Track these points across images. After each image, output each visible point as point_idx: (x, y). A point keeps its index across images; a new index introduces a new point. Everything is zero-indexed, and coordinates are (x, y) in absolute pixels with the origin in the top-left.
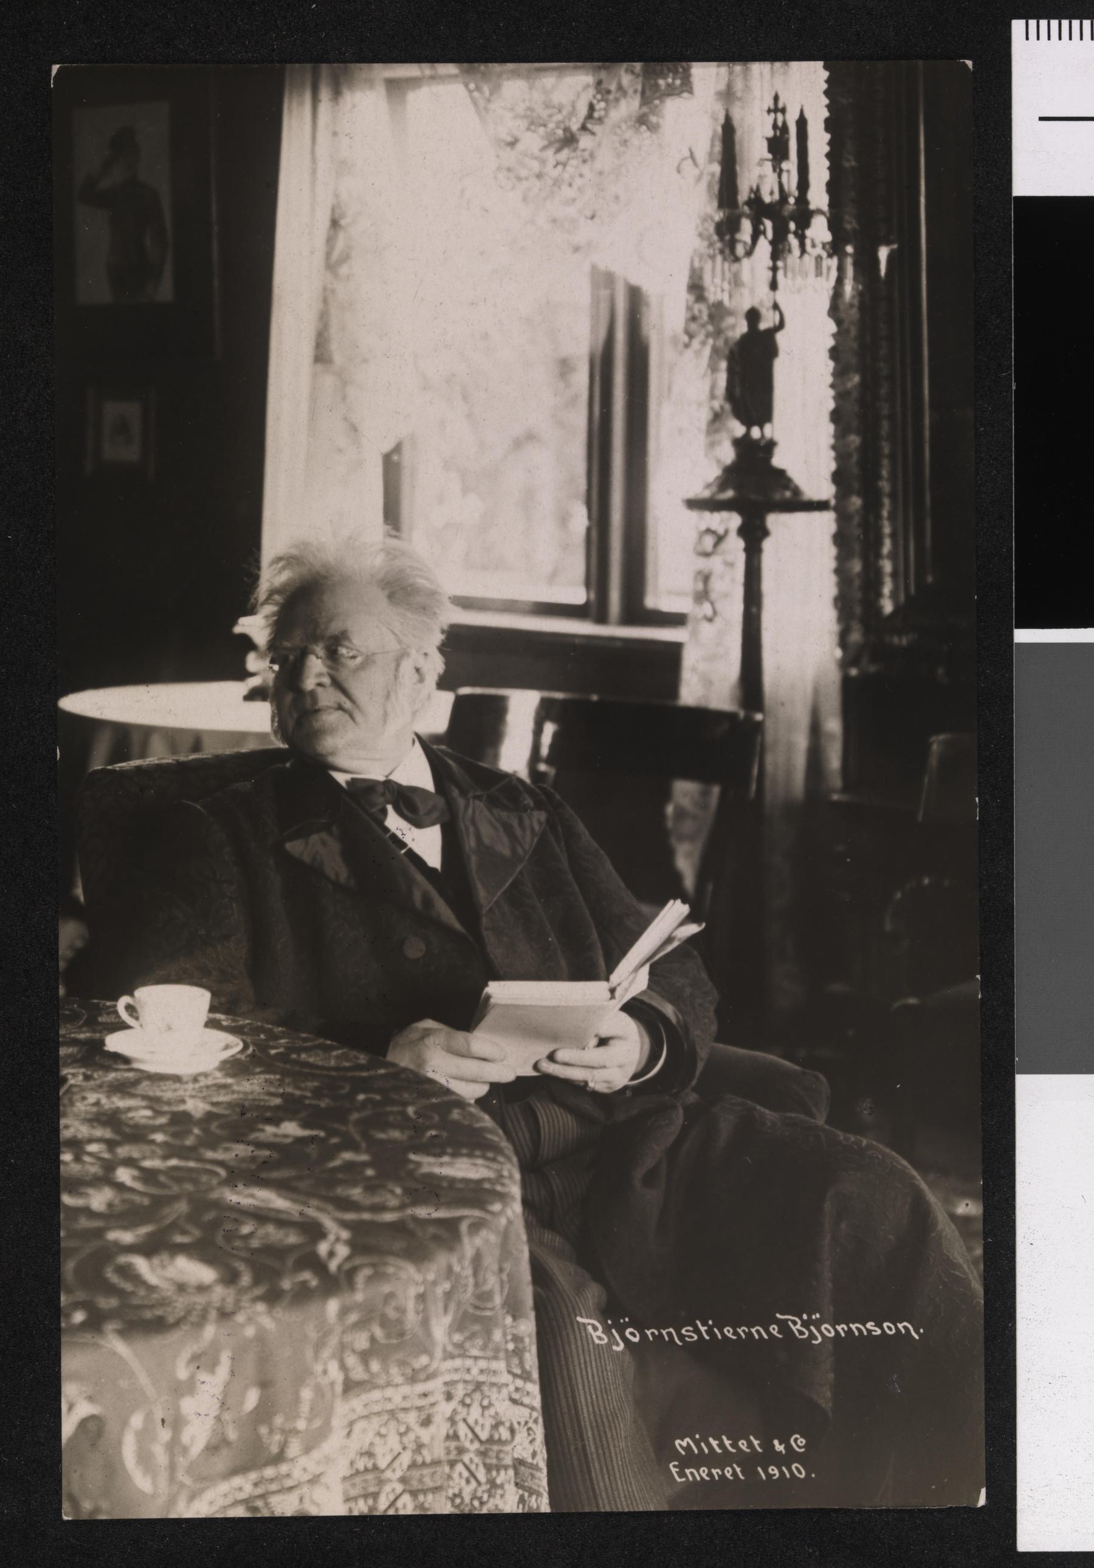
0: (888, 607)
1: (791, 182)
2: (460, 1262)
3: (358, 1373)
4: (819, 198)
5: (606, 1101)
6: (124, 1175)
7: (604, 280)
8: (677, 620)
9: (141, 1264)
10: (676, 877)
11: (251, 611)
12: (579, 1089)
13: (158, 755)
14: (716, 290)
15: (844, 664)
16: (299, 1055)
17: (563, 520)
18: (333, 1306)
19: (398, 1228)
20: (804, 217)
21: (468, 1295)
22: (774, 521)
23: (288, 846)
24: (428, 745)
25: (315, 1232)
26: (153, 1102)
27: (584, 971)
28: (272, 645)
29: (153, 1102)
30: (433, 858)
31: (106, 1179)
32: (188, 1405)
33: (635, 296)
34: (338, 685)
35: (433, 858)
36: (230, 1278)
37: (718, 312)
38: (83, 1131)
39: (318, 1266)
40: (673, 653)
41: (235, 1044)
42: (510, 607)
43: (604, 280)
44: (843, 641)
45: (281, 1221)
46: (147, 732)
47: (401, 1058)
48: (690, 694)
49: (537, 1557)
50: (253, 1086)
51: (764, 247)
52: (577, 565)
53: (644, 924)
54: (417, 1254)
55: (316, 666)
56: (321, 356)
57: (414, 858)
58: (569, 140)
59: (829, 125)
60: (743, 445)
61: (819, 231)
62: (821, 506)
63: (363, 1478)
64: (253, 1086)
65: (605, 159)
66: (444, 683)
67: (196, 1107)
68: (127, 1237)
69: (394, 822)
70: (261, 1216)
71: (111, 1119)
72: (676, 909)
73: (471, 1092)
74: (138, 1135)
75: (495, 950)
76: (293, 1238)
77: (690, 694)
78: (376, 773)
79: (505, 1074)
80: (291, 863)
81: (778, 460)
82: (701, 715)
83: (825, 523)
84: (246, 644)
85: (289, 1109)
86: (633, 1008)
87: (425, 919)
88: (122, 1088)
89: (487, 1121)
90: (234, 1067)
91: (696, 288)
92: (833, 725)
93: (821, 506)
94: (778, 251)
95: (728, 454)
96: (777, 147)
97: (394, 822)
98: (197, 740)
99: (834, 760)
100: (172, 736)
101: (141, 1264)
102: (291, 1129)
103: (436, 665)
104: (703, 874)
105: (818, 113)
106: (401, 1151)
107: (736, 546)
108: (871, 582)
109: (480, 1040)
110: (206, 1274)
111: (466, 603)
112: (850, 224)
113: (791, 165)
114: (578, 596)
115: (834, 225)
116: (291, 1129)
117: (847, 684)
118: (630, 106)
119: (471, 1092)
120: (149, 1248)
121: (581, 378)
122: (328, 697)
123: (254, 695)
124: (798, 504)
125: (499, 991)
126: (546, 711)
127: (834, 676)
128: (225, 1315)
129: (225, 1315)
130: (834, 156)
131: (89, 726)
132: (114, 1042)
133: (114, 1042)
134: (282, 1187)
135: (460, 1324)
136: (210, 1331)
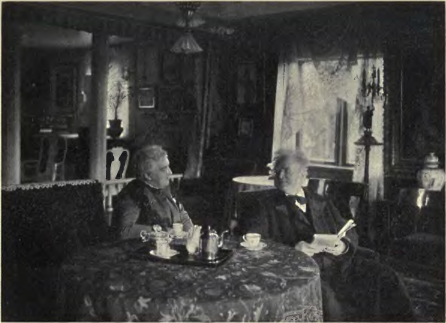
0: (393, 164)
1: (376, 82)
2: (307, 287)
3: (288, 308)
4: (381, 85)
5: (337, 257)
6: (243, 269)
7: (339, 100)
8: (352, 166)
9: (247, 287)
10: (351, 215)
11: (270, 162)
12: (331, 255)
13: (251, 190)
14: (362, 102)
15: (385, 175)
16: (236, 219)
17: (331, 146)
18: (283, 295)
19: (297, 280)
20: (379, 89)
21: (309, 294)
22: (371, 147)
23: (200, 49)
24: (304, 189)
25: (280, 281)
26: (249, 256)
27: (334, 232)
28: (275, 169)
29: (249, 256)
30: (304, 211)
31: (240, 270)
32: (255, 313)
33: (345, 103)
34: (287, 177)
35: (304, 211)
36: (263, 289)
37: (361, 107)
38: (235, 260)
39: (281, 288)
40: (351, 172)
41: (266, 245)
42: (320, 163)
43: (339, 100)
44: (384, 170)
45: (274, 279)
46: (249, 185)
47: (297, 248)
48: (355, 180)
49: (252, 76)
50: (269, 253)
51: (371, 95)
52: (333, 154)
53: (344, 224)
54: (300, 286)
55: (282, 174)
56: (285, 114)
57: (301, 211)
58: (333, 73)
59: (384, 71)
60: (365, 132)
61: (382, 91)
62: (380, 144)
63: (327, 127)
64: (269, 253)
65: (340, 77)
66: (308, 177)
67: (257, 256)
68: (243, 281)
69: (297, 203)
70: (269, 277)
71: (241, 258)
72: (351, 221)
73: (310, 254)
74: (246, 261)
75: (316, 228)
76: (275, 282)
77: (355, 180)
78: (294, 194)
79: (317, 252)
80: (277, 211)
81: (373, 135)
82: (357, 184)
83: (381, 148)
84: (269, 169)
85: (275, 257)
86: (343, 240)
87: (303, 222)
88: (243, 253)
89: (313, 261)
90: (265, 249)
91: (357, 101)
92: (382, 186)
93: (380, 144)
94: (374, 95)
95: (363, 134)
96: (374, 76)
97: (297, 203)
98: (259, 187)
99: (382, 193)
100: (254, 186)
101: (247, 287)
102: (276, 261)
103: (306, 173)
104: (357, 214)
105: (382, 69)
106: (297, 266)
107: (364, 152)
108: (390, 161)
109: (312, 245)
110: (258, 288)
111: (312, 162)
112: (388, 90)
113: (376, 79)
114: (332, 161)
115: (385, 91)
116: (276, 261)
117: (385, 179)
118: (345, 67)
119: (310, 254)
120: (248, 283)
121: (335, 119)
122: (285, 180)
123: (270, 179)
124: (376, 144)
125: (316, 236)
126: (326, 183)
127: (382, 178)
128: (262, 296)
129: (262, 296)
130: (385, 77)
131: (238, 184)
132: (242, 244)
133: (242, 244)
134: (273, 272)
135: (307, 299)
136: (260, 299)
